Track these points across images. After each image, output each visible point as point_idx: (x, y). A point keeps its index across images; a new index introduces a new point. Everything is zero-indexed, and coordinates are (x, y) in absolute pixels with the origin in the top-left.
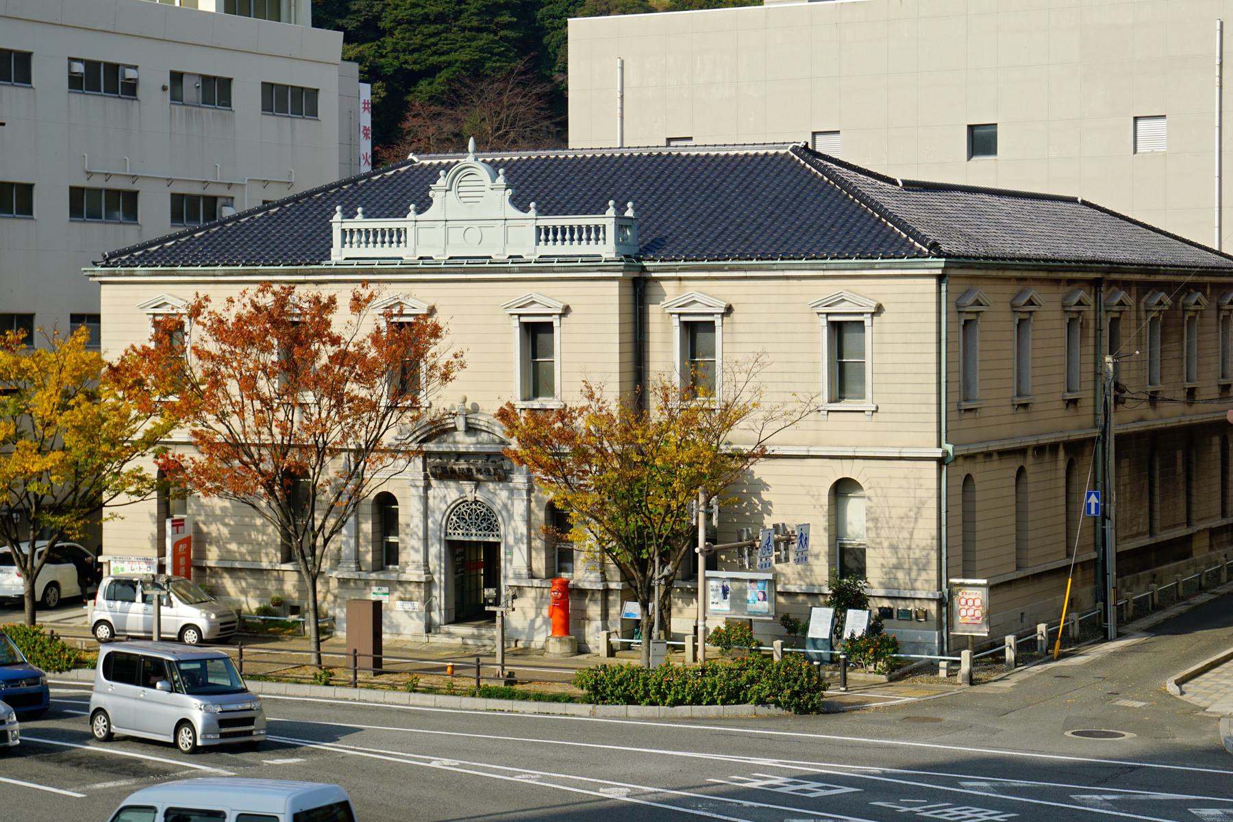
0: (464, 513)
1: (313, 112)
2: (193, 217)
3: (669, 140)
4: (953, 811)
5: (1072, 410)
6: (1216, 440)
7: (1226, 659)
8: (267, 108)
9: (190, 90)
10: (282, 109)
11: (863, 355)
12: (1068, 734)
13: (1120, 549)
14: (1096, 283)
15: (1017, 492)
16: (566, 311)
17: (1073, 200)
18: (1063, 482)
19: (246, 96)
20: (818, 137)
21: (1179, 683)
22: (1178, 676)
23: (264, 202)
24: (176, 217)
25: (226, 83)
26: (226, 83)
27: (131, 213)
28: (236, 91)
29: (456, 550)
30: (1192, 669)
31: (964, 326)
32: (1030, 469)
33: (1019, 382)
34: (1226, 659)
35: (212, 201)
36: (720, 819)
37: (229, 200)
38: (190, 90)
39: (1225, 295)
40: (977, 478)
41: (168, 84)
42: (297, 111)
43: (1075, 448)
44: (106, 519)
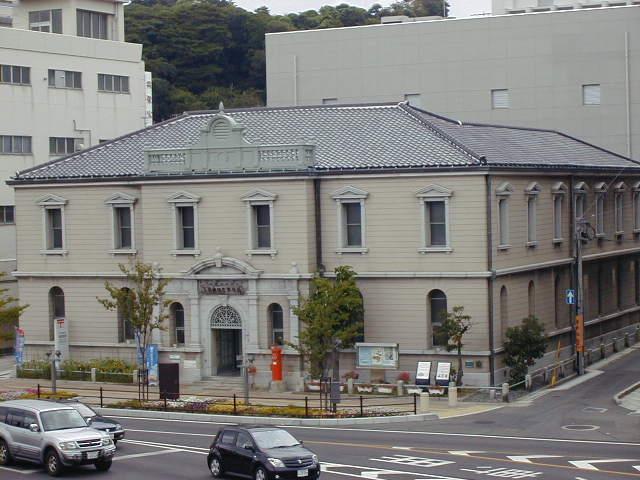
0: (221, 312)
1: (126, 90)
2: (61, 149)
3: (324, 100)
4: (506, 472)
5: (531, 253)
6: (632, 264)
7: (636, 387)
8: (101, 87)
9: (60, 78)
10: (109, 87)
11: (360, 222)
12: (564, 427)
13: (588, 323)
14: (569, 177)
15: (529, 295)
16: (67, 204)
17: (554, 132)
18: (553, 288)
19: (90, 82)
20: (496, 94)
21: (620, 397)
22: (619, 394)
23: (101, 141)
24: (52, 150)
25: (78, 75)
26: (78, 75)
27: (29, 151)
28: (84, 80)
29: (219, 335)
30: (630, 388)
31: (500, 203)
32: (536, 283)
33: (501, 237)
34: (636, 387)
35: (71, 141)
36: (239, 477)
37: (23, 143)
38: (60, 78)
39: (634, 183)
40: (507, 287)
41: (47, 77)
42: (117, 89)
43: (559, 270)
44: (167, 317)
